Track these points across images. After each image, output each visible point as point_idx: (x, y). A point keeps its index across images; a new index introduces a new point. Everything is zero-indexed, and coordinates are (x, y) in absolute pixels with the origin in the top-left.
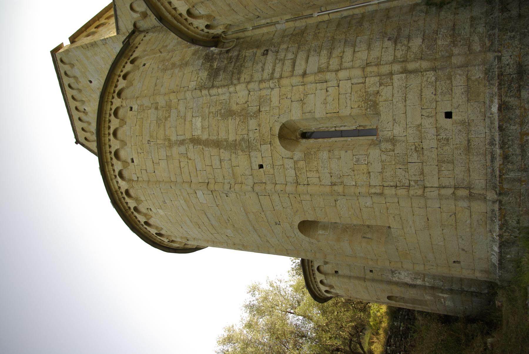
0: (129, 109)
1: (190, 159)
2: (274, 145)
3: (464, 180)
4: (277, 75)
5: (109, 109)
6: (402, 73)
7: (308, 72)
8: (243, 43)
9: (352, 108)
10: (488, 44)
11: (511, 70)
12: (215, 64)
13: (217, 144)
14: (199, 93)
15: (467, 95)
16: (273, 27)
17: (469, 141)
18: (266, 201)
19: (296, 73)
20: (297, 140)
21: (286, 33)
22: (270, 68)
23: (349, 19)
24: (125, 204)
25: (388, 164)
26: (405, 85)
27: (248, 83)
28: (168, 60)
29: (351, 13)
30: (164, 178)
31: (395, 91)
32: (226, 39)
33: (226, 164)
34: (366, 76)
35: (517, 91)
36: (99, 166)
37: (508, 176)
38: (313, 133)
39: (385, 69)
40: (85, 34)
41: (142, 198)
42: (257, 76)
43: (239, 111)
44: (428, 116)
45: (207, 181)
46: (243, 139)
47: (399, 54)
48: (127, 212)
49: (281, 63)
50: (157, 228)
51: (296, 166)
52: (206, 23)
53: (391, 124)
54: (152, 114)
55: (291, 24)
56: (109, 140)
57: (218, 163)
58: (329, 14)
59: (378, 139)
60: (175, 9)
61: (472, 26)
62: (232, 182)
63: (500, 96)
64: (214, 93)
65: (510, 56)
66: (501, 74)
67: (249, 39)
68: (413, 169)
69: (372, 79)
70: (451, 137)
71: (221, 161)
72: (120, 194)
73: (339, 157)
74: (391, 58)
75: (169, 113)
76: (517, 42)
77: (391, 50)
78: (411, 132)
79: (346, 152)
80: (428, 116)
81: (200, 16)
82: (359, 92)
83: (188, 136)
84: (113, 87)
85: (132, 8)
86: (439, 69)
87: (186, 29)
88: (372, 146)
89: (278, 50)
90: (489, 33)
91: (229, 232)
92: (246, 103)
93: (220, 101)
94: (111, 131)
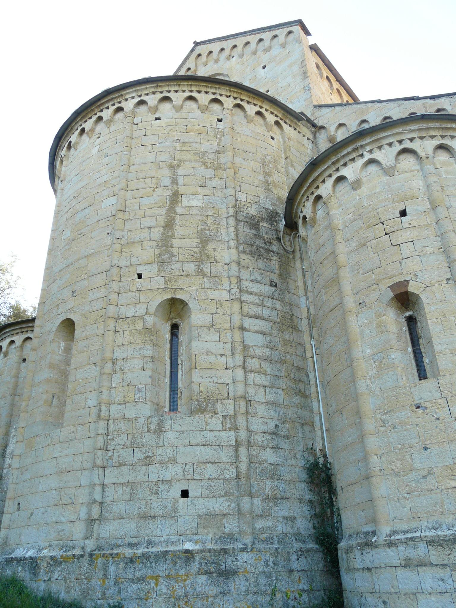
0: (220, 118)
1: (154, 190)
2: (163, 293)
3: (111, 512)
4: (245, 297)
5: (221, 92)
6: (236, 441)
7: (245, 333)
8: (287, 258)
9: (200, 384)
10: (263, 536)
11: (230, 563)
12: (265, 224)
13: (169, 225)
14: (231, 205)
15: (206, 515)
16: (303, 293)
17: (154, 517)
18: (100, 280)
19: (246, 319)
20: (169, 319)
21: (294, 308)
22: (254, 290)
23: (305, 379)
24: (106, 106)
25: (134, 425)
26: (222, 444)
27: (239, 263)
28: (275, 167)
29: (312, 382)
30: (134, 157)
31: (216, 434)
32: (294, 238)
33: (145, 234)
34: (236, 400)
35: (206, 571)
36: (152, 76)
37: (111, 563)
38: (177, 337)
39: (241, 422)
40: (321, 64)
41: (113, 128)
42: (245, 274)
43: (206, 252)
44: (185, 470)
45: (127, 210)
46: (173, 256)
47: (258, 438)
48: (96, 107)
49: (259, 302)
50: (77, 143)
51: (137, 318)
52: (308, 217)
53: (179, 428)
54: (211, 146)
55: (305, 314)
56: (184, 91)
57: (147, 225)
58: (313, 357)
59: (164, 414)
60: (324, 181)
61: (285, 518)
62: (124, 241)
63: (202, 551)
64: (229, 223)
65: (246, 562)
66: (225, 551)
67: (292, 264)
68: (126, 455)
69: (232, 407)
70: (159, 497)
71: (150, 228)
72: (118, 100)
73: (145, 368)
74: (254, 428)
75: (210, 168)
76: (261, 568)
77: (264, 428)
79: (150, 377)
80: (185, 470)
81: (315, 211)
82: (217, 392)
83: (182, 189)
84: (248, 99)
85: (341, 125)
86: (238, 482)
87: (302, 192)
88: (155, 407)
89: (274, 299)
90: (275, 537)
91: (68, 234)
92: (215, 260)
93: (219, 230)
94: (195, 94)
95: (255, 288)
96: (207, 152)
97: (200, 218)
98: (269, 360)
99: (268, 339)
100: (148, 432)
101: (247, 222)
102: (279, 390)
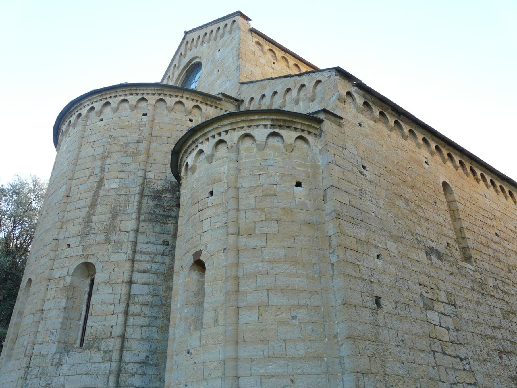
0: (145, 112)
1: (89, 178)
2: (80, 258)
13: (93, 205)
26: (100, 373)
31: (96, 365)
40: (262, 41)
43: (114, 224)
49: (150, 259)
53: (71, 362)
75: (130, 156)
77: (137, 359)
78: (61, 380)
82: (103, 333)
87: (313, 125)
93: (127, 205)
95: (149, 248)
96: (130, 143)
97: (114, 197)
98: (150, 305)
99: (152, 288)
100: (52, 365)
101: (151, 196)
102: (154, 328)
